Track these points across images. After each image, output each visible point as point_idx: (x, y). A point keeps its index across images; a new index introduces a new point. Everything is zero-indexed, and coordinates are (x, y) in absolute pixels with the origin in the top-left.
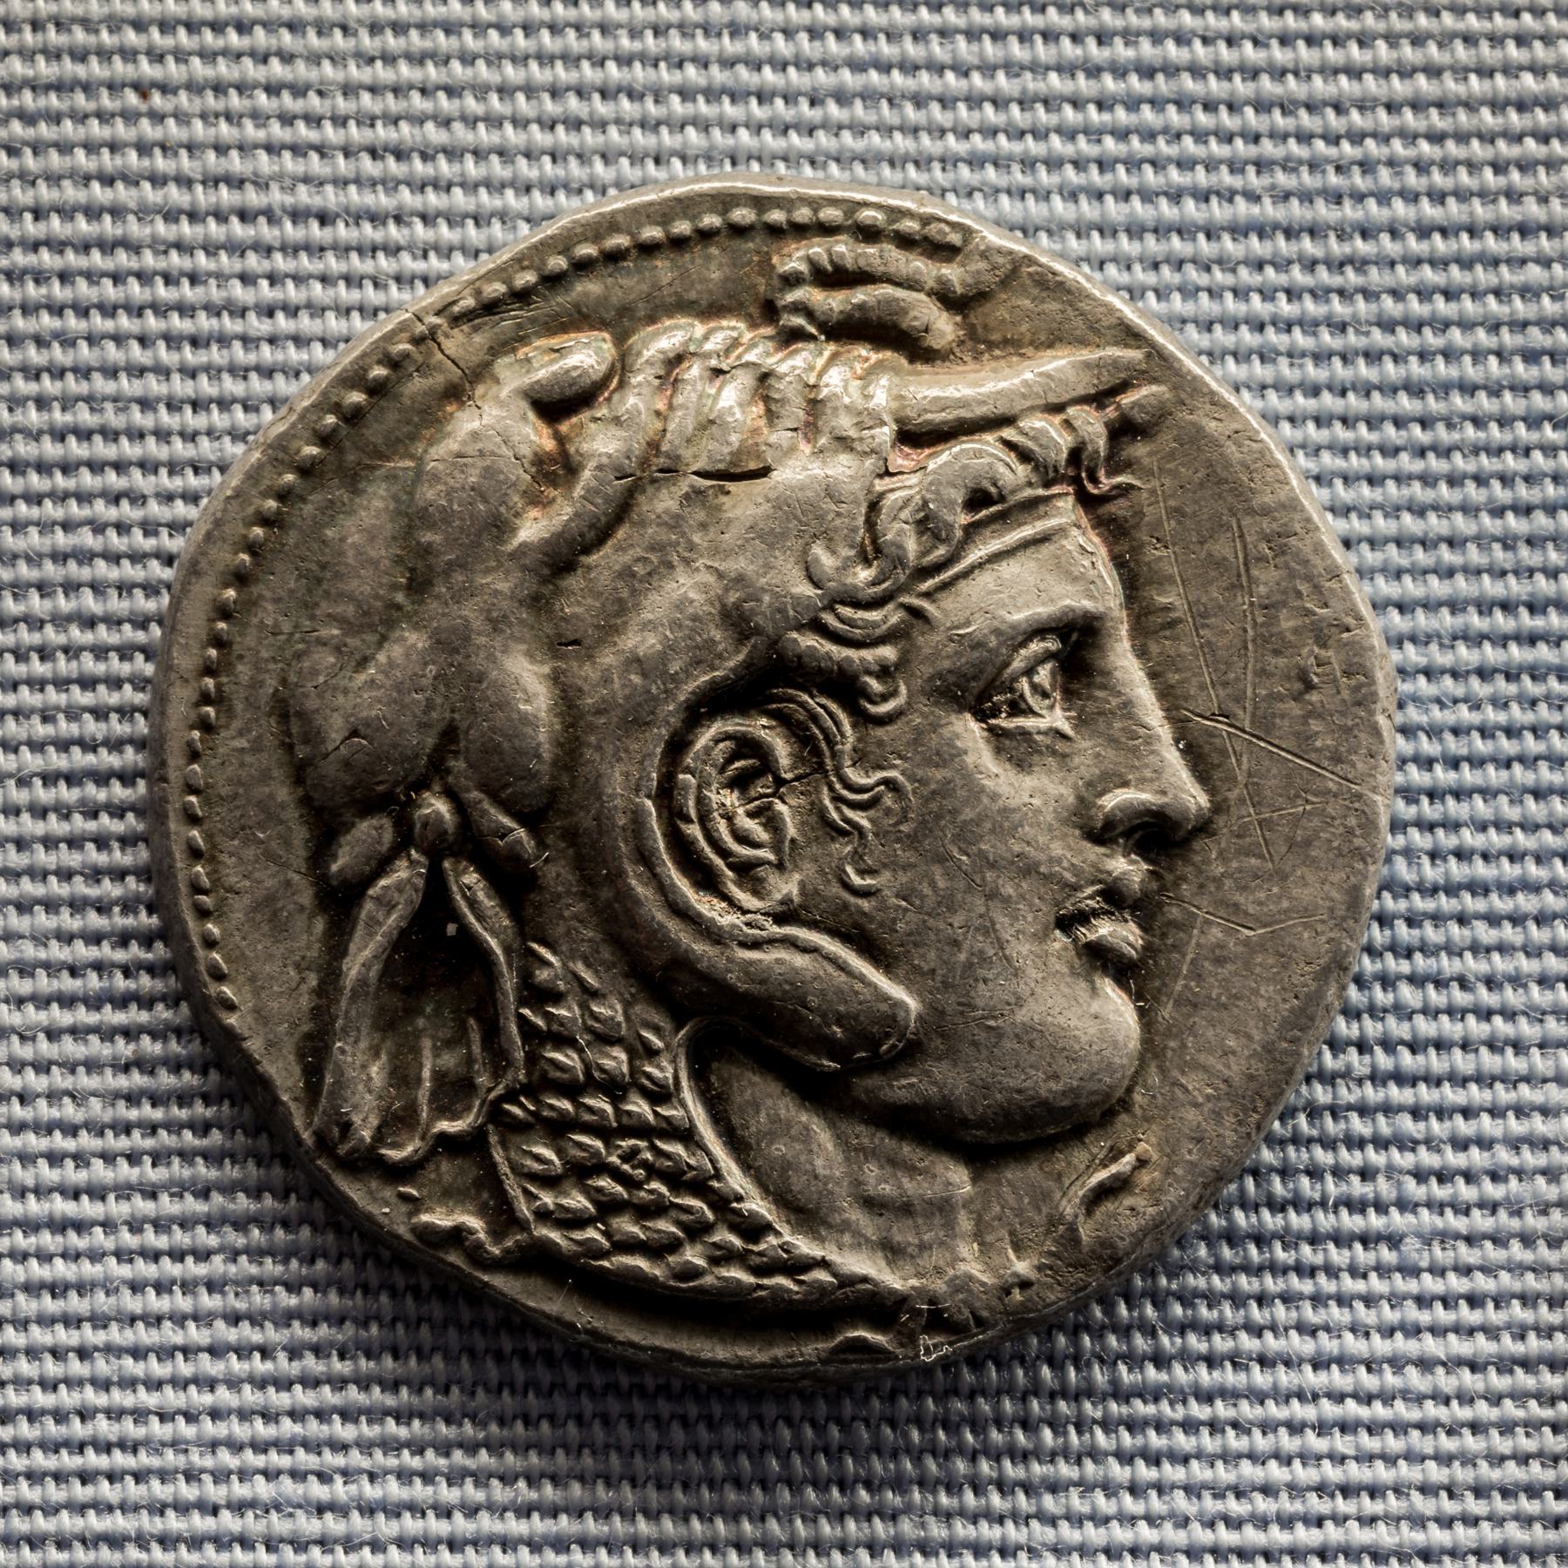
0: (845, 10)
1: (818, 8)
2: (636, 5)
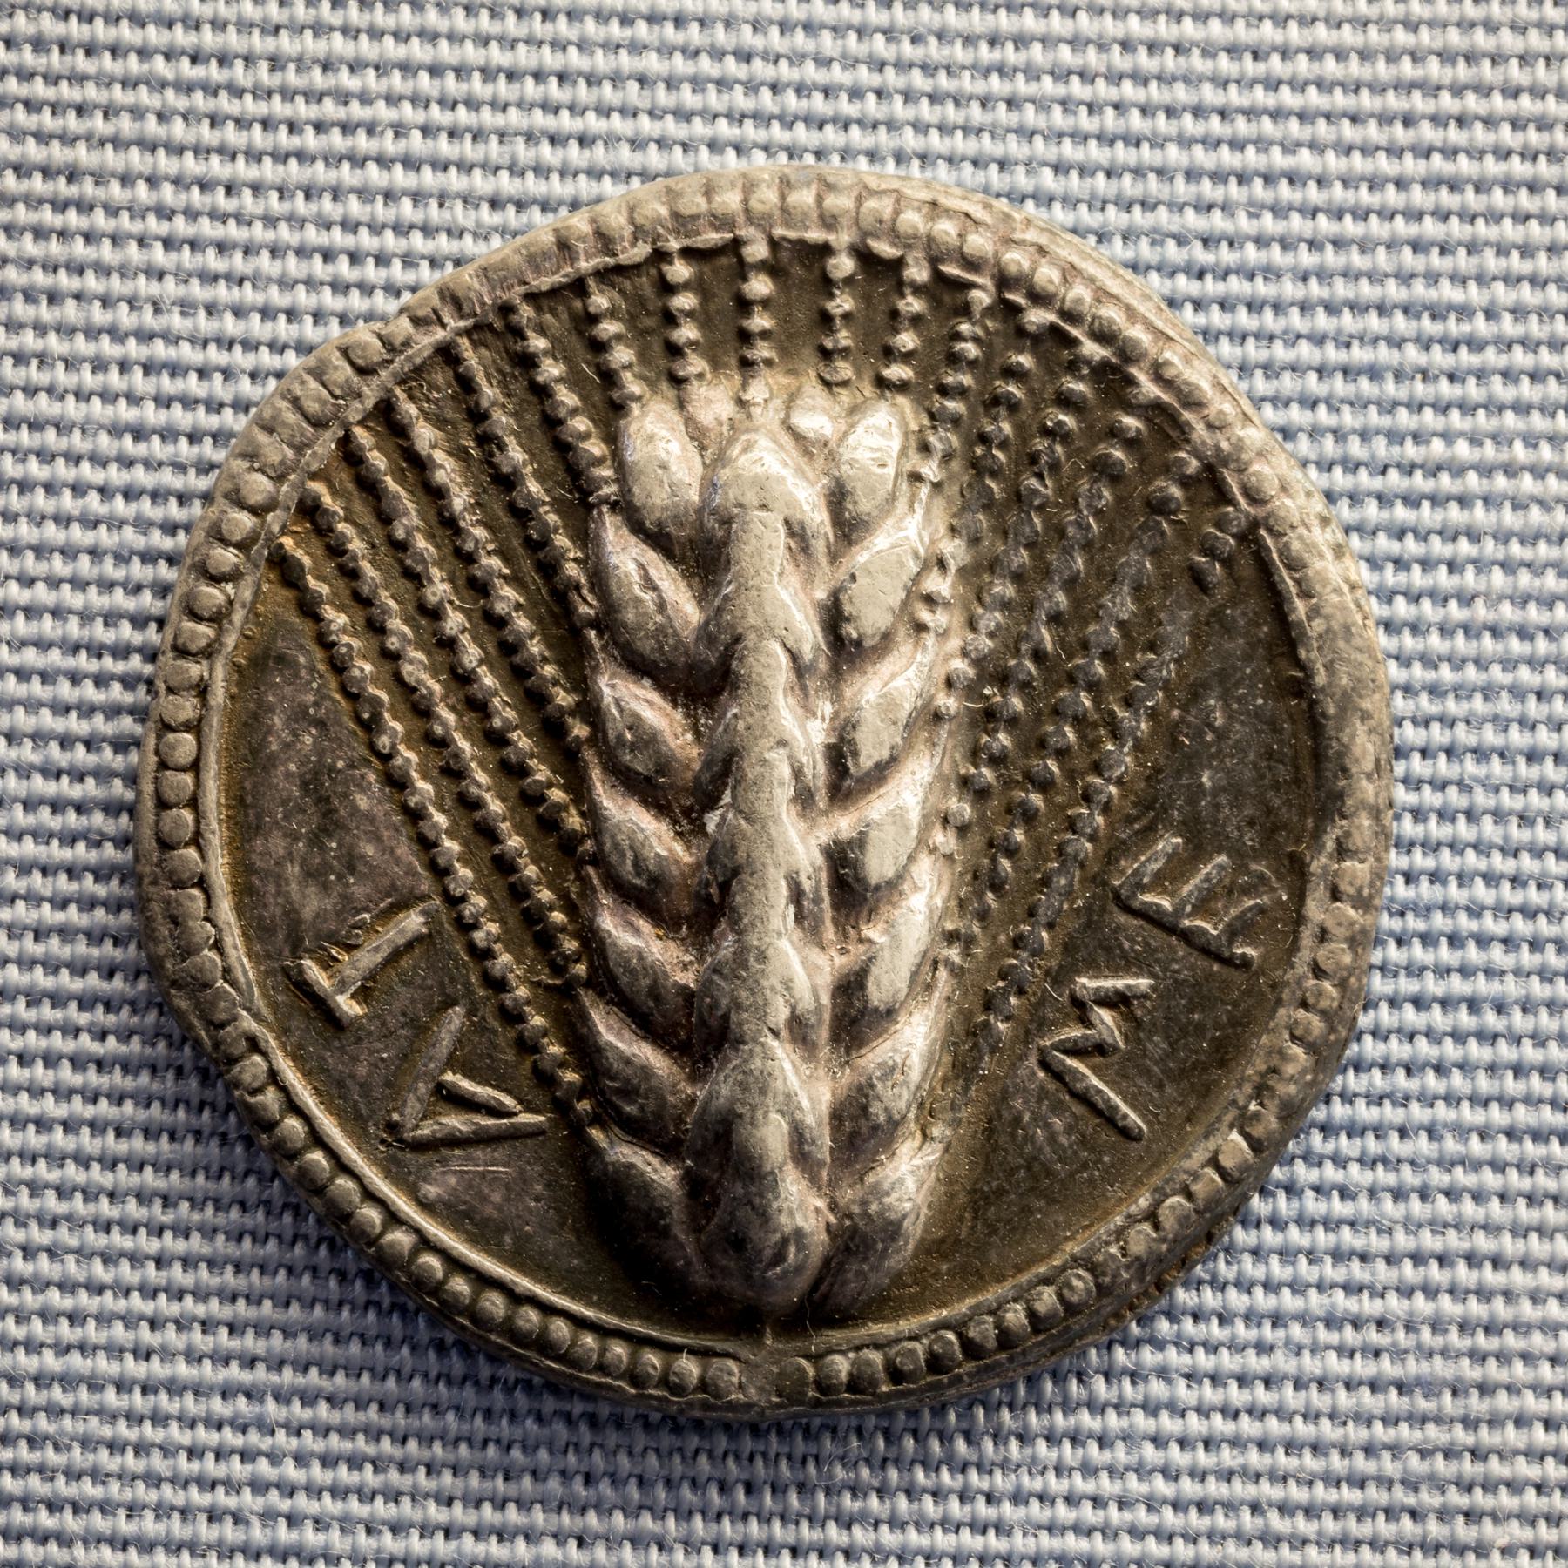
0: (925, 12)
2: (898, 7)
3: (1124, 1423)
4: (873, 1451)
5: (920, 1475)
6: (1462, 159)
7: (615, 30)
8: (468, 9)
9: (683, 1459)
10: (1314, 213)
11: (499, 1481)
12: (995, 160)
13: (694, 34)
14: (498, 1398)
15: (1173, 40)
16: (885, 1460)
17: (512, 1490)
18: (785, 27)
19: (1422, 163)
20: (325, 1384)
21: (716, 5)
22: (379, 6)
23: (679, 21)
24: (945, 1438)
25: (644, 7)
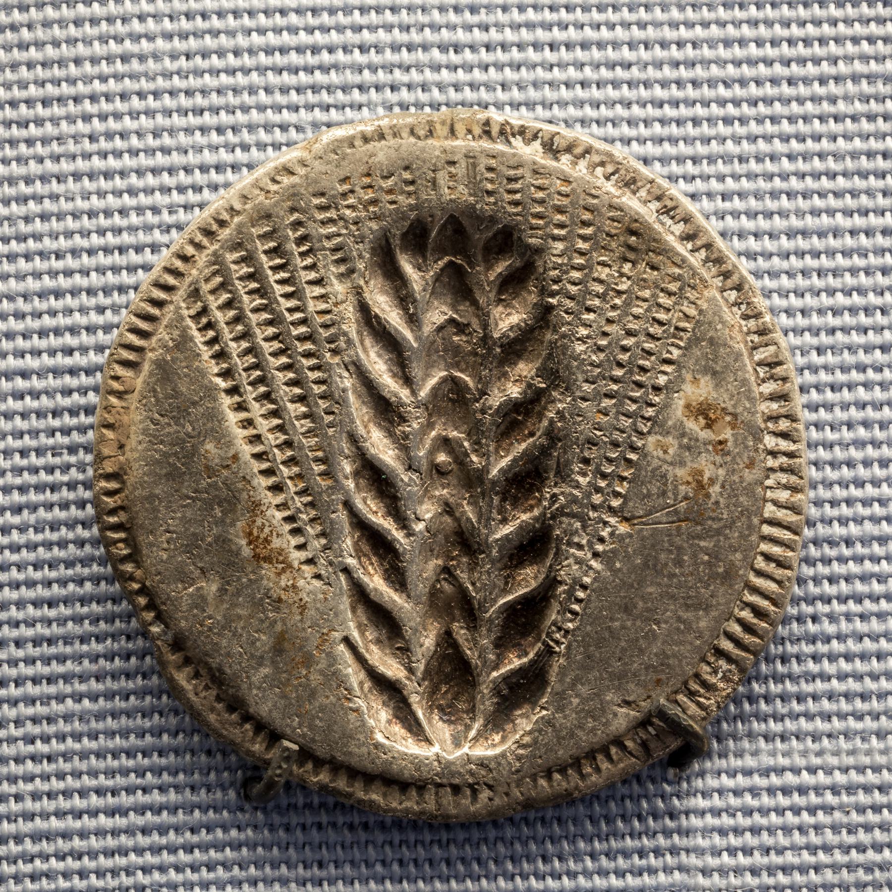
0: (81, 7)
1: (96, 5)
2: (111, 4)
3: (20, 848)
4: (567, 831)
5: (582, 845)
6: (444, 72)
7: (310, 20)
8: (790, 4)
9: (408, 847)
10: (201, 112)
11: (315, 869)
12: (404, 85)
13: (325, 18)
14: (294, 820)
15: (104, 16)
16: (575, 836)
17: (324, 874)
18: (189, 16)
19: (293, 77)
20: (173, 820)
21: (242, 4)
22: (864, 4)
23: (283, 12)
24: (609, 820)
25: (294, 5)
